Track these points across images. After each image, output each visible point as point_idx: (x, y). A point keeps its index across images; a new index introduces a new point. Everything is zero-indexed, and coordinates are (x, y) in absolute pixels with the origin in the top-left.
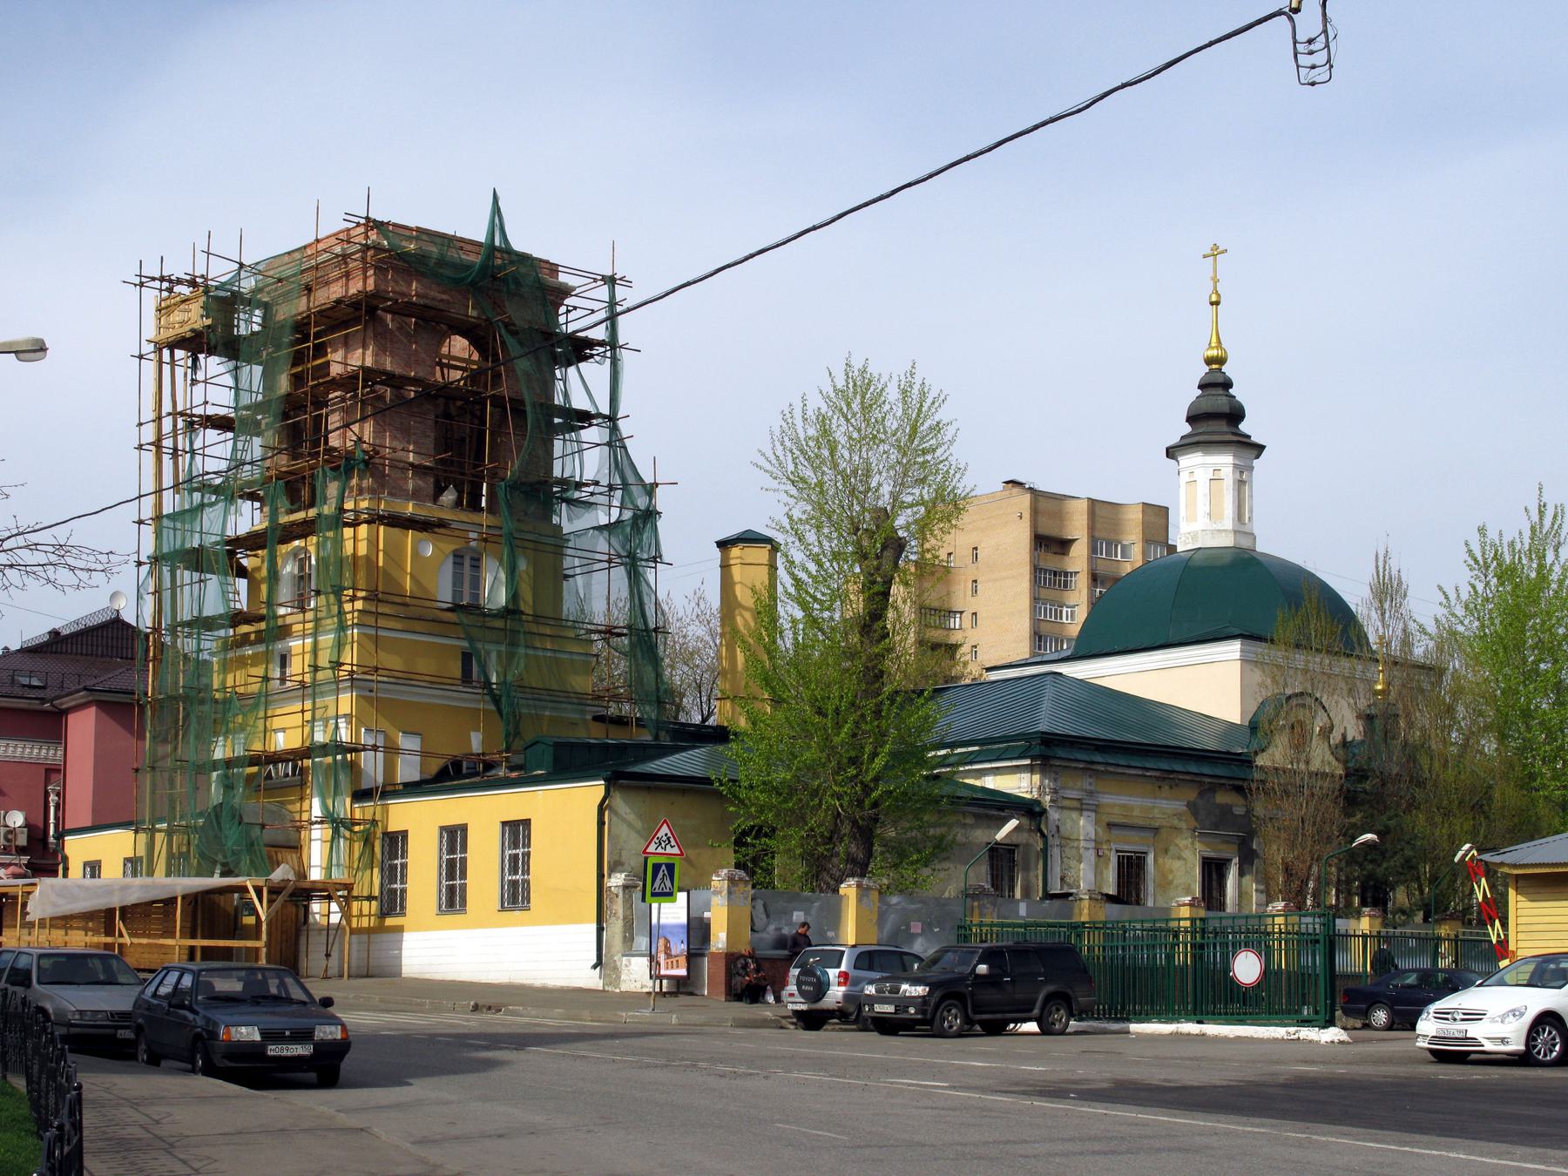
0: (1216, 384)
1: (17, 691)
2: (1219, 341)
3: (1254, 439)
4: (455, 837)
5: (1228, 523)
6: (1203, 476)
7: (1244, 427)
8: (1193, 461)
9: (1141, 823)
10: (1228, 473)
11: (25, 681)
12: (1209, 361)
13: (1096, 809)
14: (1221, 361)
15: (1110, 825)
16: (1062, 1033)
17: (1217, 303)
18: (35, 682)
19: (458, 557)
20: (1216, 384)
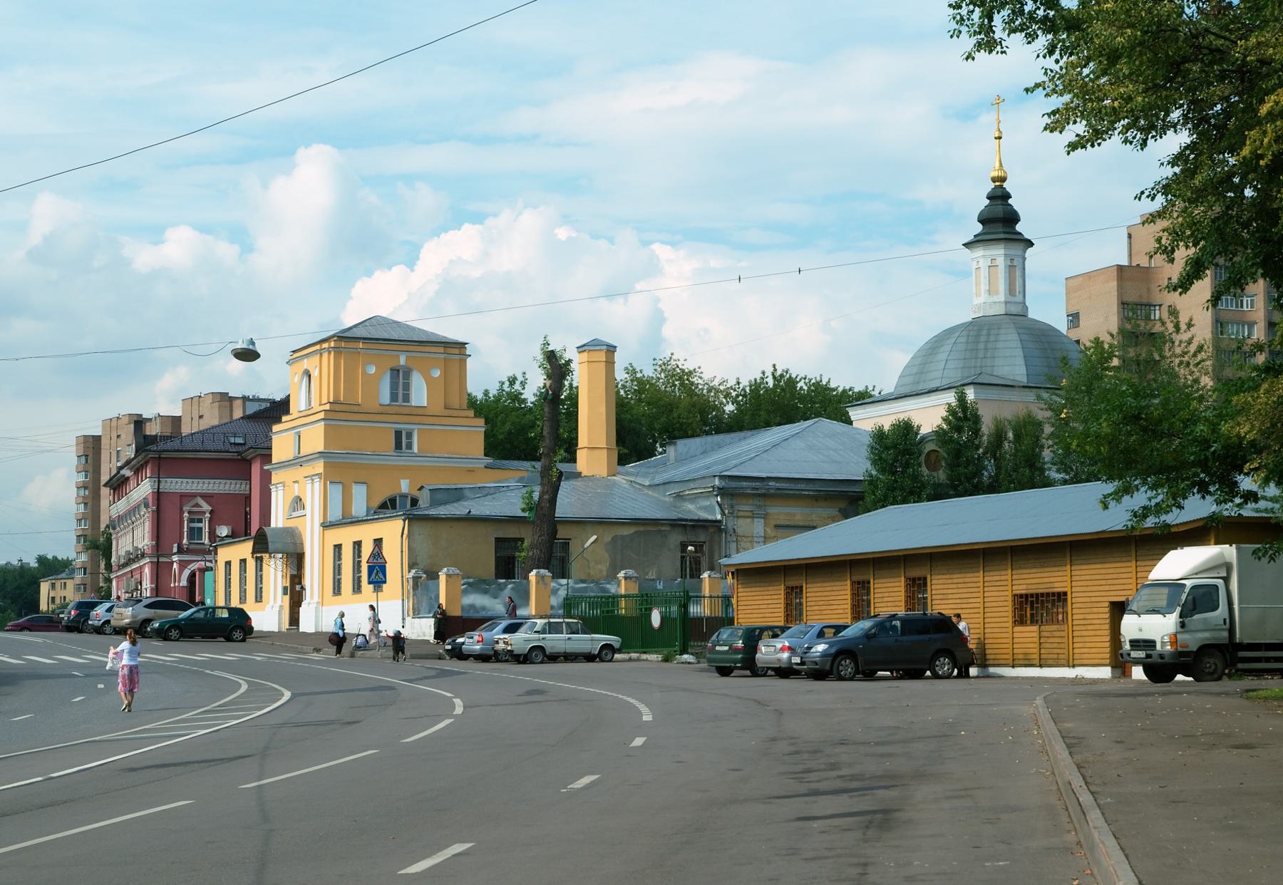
0: (1000, 196)
1: (228, 447)
2: (1001, 165)
3: (1027, 236)
4: (358, 545)
5: (1001, 297)
6: (984, 264)
7: (1019, 228)
8: (979, 252)
9: (801, 524)
10: (1001, 261)
11: (232, 440)
12: (994, 180)
13: (765, 517)
14: (1003, 179)
15: (777, 526)
16: (610, 661)
17: (1000, 138)
18: (240, 441)
19: (395, 371)
20: (1000, 196)
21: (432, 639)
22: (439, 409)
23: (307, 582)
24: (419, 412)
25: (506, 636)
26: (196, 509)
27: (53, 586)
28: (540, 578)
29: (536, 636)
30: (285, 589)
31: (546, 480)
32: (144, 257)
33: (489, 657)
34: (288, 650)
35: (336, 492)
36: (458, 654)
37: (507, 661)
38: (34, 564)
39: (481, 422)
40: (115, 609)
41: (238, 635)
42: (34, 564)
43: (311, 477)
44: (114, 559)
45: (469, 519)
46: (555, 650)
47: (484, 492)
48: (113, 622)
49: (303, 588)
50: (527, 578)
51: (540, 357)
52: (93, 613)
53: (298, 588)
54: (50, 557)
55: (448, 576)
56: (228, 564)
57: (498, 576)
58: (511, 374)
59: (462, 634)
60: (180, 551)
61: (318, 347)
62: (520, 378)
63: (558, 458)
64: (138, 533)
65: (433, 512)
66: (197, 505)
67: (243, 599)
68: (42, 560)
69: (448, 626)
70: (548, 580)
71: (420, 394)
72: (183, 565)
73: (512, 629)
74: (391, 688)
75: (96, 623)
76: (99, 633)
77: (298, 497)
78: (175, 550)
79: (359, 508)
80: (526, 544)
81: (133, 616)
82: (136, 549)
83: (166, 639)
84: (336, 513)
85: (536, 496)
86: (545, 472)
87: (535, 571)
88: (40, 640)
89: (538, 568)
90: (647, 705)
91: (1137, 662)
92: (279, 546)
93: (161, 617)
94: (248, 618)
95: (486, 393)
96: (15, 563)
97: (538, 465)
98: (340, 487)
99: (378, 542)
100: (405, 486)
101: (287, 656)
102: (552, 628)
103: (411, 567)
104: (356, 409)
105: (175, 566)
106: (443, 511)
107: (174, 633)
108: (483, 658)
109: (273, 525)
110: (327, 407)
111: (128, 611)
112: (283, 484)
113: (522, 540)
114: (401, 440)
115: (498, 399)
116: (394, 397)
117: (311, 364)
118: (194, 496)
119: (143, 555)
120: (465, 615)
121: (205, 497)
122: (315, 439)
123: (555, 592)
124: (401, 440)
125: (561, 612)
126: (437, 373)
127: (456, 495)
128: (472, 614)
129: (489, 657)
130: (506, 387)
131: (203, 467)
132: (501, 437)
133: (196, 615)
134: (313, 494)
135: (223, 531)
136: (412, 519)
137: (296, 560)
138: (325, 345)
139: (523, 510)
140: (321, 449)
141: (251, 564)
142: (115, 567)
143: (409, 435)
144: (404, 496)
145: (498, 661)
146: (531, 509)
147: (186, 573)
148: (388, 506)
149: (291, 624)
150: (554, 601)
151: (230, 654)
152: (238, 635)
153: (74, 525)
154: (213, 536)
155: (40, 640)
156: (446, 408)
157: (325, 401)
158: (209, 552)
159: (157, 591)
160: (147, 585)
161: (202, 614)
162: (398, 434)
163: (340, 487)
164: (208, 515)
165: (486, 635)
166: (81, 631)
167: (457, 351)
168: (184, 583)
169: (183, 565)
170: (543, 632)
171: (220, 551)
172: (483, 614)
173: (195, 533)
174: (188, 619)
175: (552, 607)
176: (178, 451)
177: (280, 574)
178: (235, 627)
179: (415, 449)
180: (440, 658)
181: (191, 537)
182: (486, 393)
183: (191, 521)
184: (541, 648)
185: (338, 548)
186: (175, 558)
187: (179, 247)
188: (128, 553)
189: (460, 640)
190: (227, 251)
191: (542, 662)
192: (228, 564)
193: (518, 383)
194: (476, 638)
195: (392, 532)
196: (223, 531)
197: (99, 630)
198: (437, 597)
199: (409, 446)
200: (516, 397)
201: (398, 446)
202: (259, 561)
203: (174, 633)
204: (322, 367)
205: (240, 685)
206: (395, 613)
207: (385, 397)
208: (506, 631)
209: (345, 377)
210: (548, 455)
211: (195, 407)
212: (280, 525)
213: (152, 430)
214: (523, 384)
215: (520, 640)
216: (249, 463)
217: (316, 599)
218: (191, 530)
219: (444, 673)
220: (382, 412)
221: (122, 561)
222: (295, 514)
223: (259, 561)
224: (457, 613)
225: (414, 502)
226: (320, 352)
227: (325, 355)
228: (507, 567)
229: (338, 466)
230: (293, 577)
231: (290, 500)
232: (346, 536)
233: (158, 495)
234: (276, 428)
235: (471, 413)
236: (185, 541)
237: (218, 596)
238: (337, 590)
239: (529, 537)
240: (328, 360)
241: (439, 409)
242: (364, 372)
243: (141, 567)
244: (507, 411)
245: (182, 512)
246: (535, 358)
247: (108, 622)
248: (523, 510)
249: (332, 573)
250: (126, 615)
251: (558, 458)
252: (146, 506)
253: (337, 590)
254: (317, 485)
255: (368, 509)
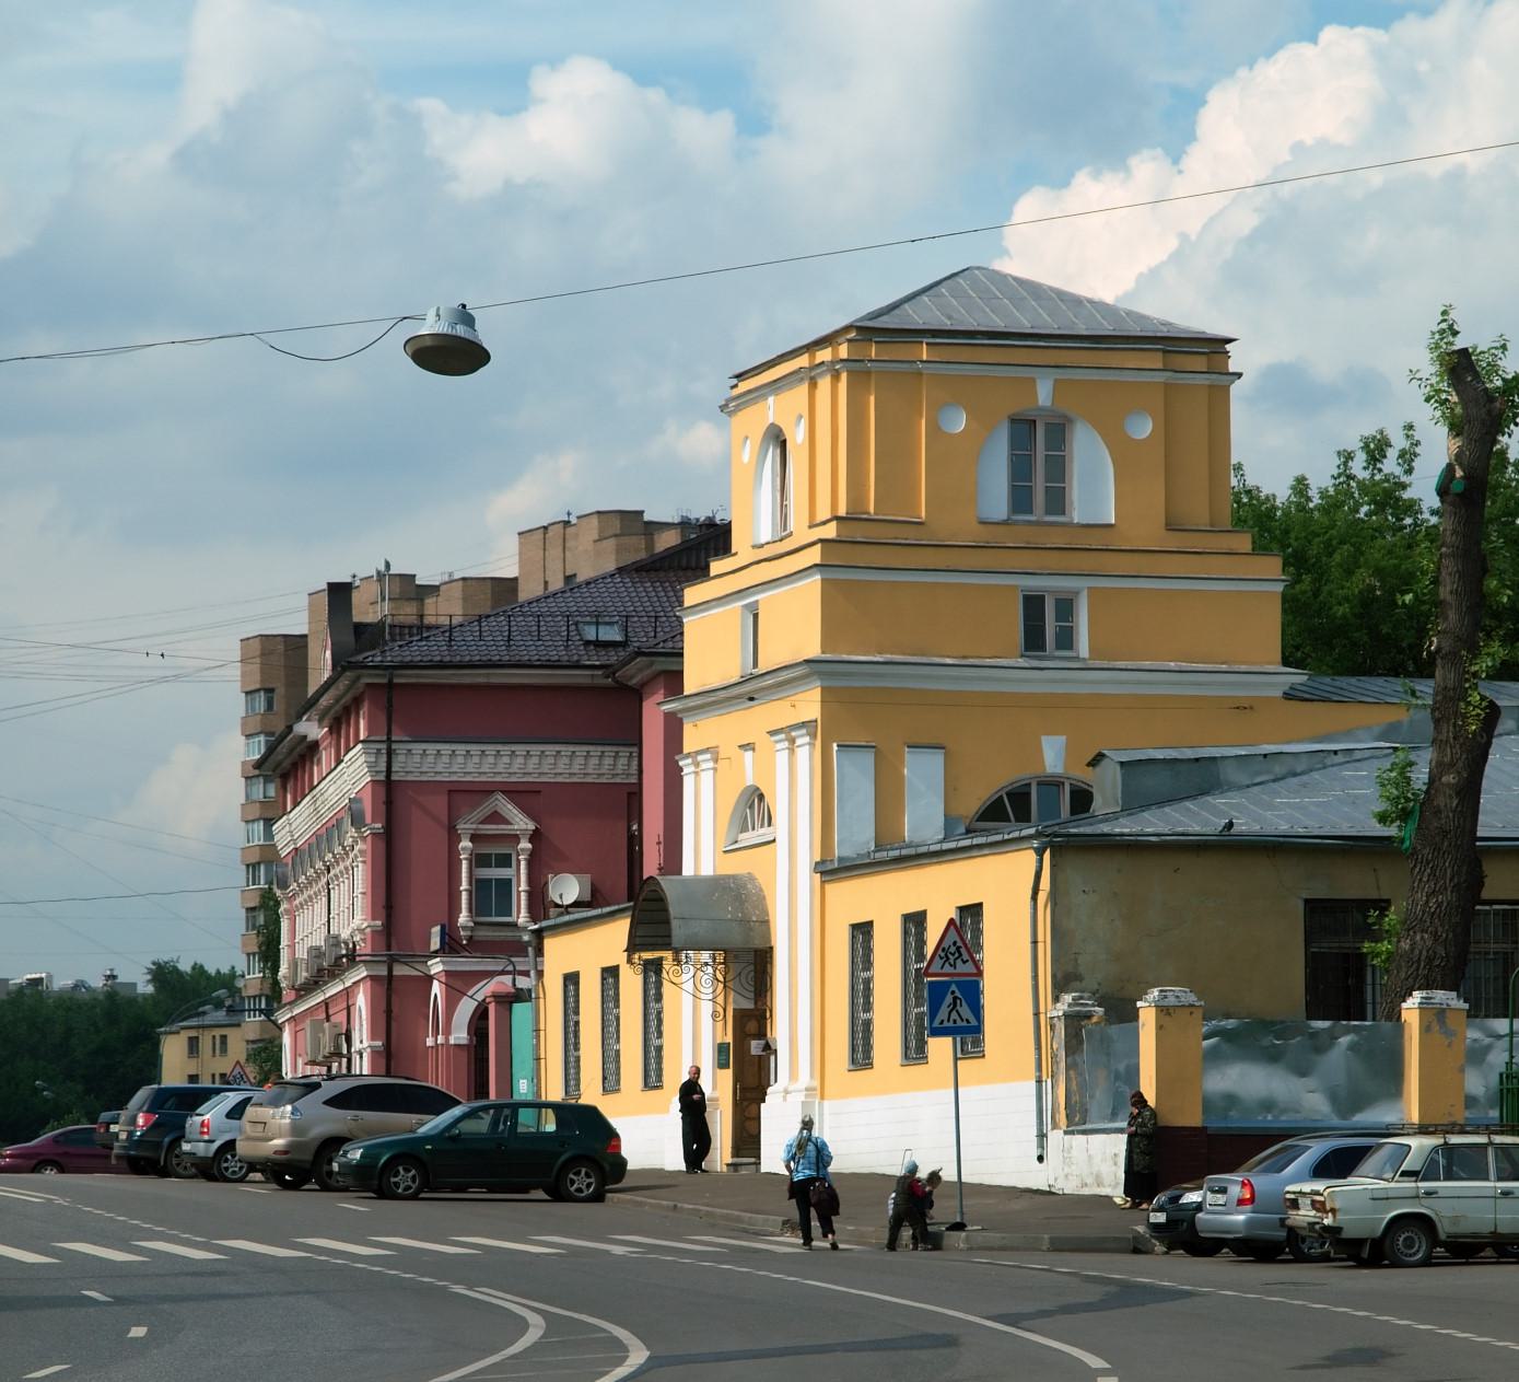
1: (578, 653)
11: (590, 633)
18: (612, 634)
19: (1023, 427)
21: (1118, 1195)
22: (1149, 532)
23: (780, 1031)
24: (1095, 544)
25: (1319, 1185)
26: (491, 829)
27: (193, 1045)
28: (1434, 1017)
29: (1409, 1184)
30: (722, 1049)
31: (1448, 732)
32: (485, 153)
33: (1274, 1245)
34: (713, 1226)
35: (858, 776)
36: (1185, 1236)
37: (1325, 1258)
38: (145, 988)
39: (1272, 566)
40: (250, 1111)
41: (581, 1181)
42: (145, 988)
43: (787, 732)
44: (283, 970)
45: (1229, 847)
46: (1464, 1228)
47: (1276, 769)
48: (242, 1148)
49: (769, 1049)
50: (1394, 1015)
51: (1428, 368)
52: (194, 1122)
53: (755, 1047)
54: (185, 966)
55: (1163, 1010)
56: (572, 980)
57: (1317, 1006)
58: (1370, 431)
59: (1195, 1177)
60: (450, 945)
61: (803, 361)
62: (1399, 442)
63: (1484, 664)
64: (340, 895)
65: (1124, 827)
66: (496, 817)
67: (611, 1082)
68: (163, 974)
69: (1164, 1156)
70: (1456, 1021)
71: (1096, 489)
72: (458, 984)
73: (1338, 1164)
74: (946, 1341)
75: (202, 1149)
76: (211, 1178)
77: (750, 793)
78: (435, 944)
79: (923, 818)
80: (1392, 917)
81: (296, 1129)
82: (334, 941)
83: (384, 1193)
84: (858, 835)
85: (1420, 777)
86: (1447, 709)
87: (1417, 996)
88: (35, 1198)
89: (1427, 985)
90: (625, 1327)
91: (233, 1001)
92: (700, 929)
93: (372, 1132)
94: (611, 1135)
95: (1300, 486)
96: (97, 983)
97: (1426, 688)
98: (868, 759)
99: (972, 912)
100: (1053, 755)
101: (703, 1243)
102: (1454, 1163)
103: (1059, 987)
104: (911, 536)
105: (436, 988)
106: (1153, 823)
107: (404, 1178)
108: (1256, 1248)
109: (688, 869)
110: (830, 531)
111: (282, 1117)
112: (713, 752)
113: (1382, 905)
114: (1041, 626)
115: (1332, 504)
116: (1020, 499)
117: (782, 409)
118: (483, 791)
119: (352, 958)
120: (1216, 1124)
121: (522, 794)
122: (796, 624)
123: (1477, 1056)
124: (1041, 626)
125: (1494, 1114)
126: (1143, 428)
127: (1201, 778)
128: (1236, 1121)
129: (1274, 1245)
130: (1358, 467)
131: (503, 713)
132: (1341, 610)
133: (469, 1126)
134: (793, 778)
135: (567, 889)
136: (1063, 848)
137: (750, 969)
138: (824, 355)
139: (1383, 818)
140: (813, 650)
141: (631, 983)
142: (288, 995)
143: (1066, 608)
144: (1051, 784)
145: (1301, 1258)
146: (1404, 815)
147: (466, 1008)
148: (1003, 814)
149: (737, 1152)
150: (1478, 1083)
151: (536, 1235)
152: (581, 1181)
153: (240, 876)
154: (539, 903)
155: (35, 1198)
156: (1171, 526)
157: (824, 513)
158: (518, 949)
159: (387, 1056)
160: (363, 1039)
161: (482, 1125)
162: (1033, 605)
163: (868, 759)
164: (525, 845)
165: (1263, 1182)
166: (164, 1173)
167: (1200, 363)
168: (460, 1035)
169: (458, 984)
170: (1428, 1172)
171: (550, 944)
172: (1268, 1120)
173: (492, 896)
174: (445, 1137)
175: (1471, 1101)
176: (442, 666)
177: (707, 1008)
178: (579, 1155)
179: (1083, 645)
180: (1137, 1248)
181: (478, 908)
182: (1300, 486)
183: (479, 860)
184: (1423, 1222)
185: (862, 932)
186: (436, 966)
187: (569, 122)
188: (316, 953)
189: (1192, 1197)
190: (703, 133)
191: (1427, 1263)
192: (572, 980)
193: (1392, 454)
194: (1236, 1191)
195: (1006, 886)
196: (567, 889)
197: (212, 1169)
198: (1133, 1073)
199: (1066, 639)
200: (1388, 497)
201: (1034, 640)
202: (653, 969)
203: (404, 1178)
204: (814, 416)
205: (522, 1326)
206: (995, 1124)
207: (997, 502)
208: (1324, 1169)
209: (881, 447)
210: (1453, 658)
211: (554, 552)
212: (707, 870)
213: (368, 609)
214: (1408, 458)
215: (1362, 1198)
216: (633, 697)
217: (805, 1078)
218: (480, 887)
219: (1129, 1295)
220: (987, 545)
221: (303, 975)
222: (747, 838)
223: (653, 969)
224: (1192, 1118)
225: (1082, 800)
226: (810, 376)
227: (824, 384)
228: (1341, 986)
229: (862, 703)
230: (741, 1017)
231: (731, 798)
232: (884, 899)
233: (389, 790)
234: (693, 594)
235: (1244, 542)
236: (463, 918)
237: (542, 1076)
238: (861, 1054)
239: (1406, 904)
240: (831, 396)
241: (1149, 532)
242: (935, 431)
243: (348, 993)
244: (1358, 535)
245: (453, 837)
246: (1413, 376)
247: (230, 1146)
248: (1383, 818)
249: (854, 1004)
250: (275, 1126)
251: (1484, 664)
252: (357, 820)
253: (861, 1054)
254: (803, 754)
255: (950, 822)
